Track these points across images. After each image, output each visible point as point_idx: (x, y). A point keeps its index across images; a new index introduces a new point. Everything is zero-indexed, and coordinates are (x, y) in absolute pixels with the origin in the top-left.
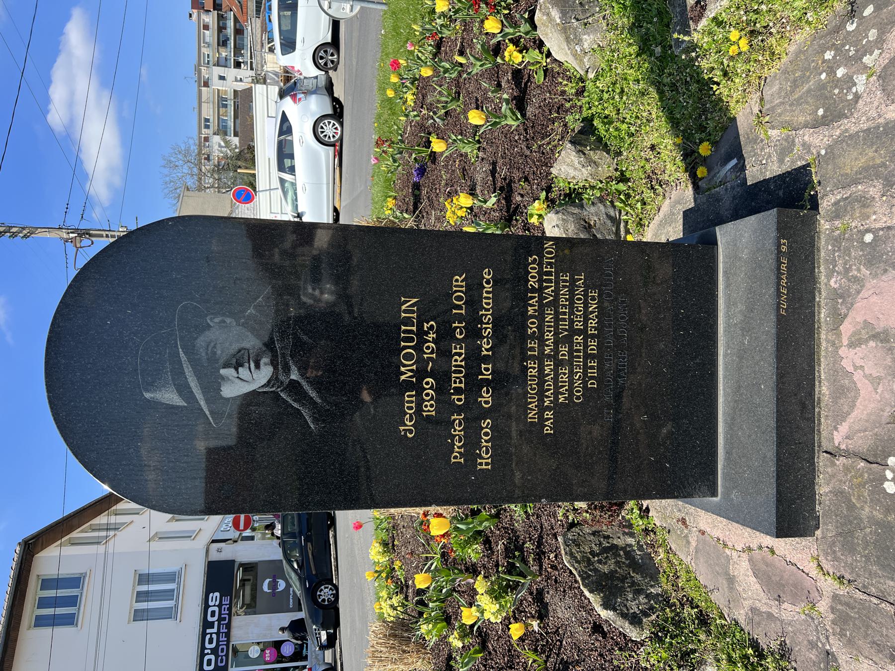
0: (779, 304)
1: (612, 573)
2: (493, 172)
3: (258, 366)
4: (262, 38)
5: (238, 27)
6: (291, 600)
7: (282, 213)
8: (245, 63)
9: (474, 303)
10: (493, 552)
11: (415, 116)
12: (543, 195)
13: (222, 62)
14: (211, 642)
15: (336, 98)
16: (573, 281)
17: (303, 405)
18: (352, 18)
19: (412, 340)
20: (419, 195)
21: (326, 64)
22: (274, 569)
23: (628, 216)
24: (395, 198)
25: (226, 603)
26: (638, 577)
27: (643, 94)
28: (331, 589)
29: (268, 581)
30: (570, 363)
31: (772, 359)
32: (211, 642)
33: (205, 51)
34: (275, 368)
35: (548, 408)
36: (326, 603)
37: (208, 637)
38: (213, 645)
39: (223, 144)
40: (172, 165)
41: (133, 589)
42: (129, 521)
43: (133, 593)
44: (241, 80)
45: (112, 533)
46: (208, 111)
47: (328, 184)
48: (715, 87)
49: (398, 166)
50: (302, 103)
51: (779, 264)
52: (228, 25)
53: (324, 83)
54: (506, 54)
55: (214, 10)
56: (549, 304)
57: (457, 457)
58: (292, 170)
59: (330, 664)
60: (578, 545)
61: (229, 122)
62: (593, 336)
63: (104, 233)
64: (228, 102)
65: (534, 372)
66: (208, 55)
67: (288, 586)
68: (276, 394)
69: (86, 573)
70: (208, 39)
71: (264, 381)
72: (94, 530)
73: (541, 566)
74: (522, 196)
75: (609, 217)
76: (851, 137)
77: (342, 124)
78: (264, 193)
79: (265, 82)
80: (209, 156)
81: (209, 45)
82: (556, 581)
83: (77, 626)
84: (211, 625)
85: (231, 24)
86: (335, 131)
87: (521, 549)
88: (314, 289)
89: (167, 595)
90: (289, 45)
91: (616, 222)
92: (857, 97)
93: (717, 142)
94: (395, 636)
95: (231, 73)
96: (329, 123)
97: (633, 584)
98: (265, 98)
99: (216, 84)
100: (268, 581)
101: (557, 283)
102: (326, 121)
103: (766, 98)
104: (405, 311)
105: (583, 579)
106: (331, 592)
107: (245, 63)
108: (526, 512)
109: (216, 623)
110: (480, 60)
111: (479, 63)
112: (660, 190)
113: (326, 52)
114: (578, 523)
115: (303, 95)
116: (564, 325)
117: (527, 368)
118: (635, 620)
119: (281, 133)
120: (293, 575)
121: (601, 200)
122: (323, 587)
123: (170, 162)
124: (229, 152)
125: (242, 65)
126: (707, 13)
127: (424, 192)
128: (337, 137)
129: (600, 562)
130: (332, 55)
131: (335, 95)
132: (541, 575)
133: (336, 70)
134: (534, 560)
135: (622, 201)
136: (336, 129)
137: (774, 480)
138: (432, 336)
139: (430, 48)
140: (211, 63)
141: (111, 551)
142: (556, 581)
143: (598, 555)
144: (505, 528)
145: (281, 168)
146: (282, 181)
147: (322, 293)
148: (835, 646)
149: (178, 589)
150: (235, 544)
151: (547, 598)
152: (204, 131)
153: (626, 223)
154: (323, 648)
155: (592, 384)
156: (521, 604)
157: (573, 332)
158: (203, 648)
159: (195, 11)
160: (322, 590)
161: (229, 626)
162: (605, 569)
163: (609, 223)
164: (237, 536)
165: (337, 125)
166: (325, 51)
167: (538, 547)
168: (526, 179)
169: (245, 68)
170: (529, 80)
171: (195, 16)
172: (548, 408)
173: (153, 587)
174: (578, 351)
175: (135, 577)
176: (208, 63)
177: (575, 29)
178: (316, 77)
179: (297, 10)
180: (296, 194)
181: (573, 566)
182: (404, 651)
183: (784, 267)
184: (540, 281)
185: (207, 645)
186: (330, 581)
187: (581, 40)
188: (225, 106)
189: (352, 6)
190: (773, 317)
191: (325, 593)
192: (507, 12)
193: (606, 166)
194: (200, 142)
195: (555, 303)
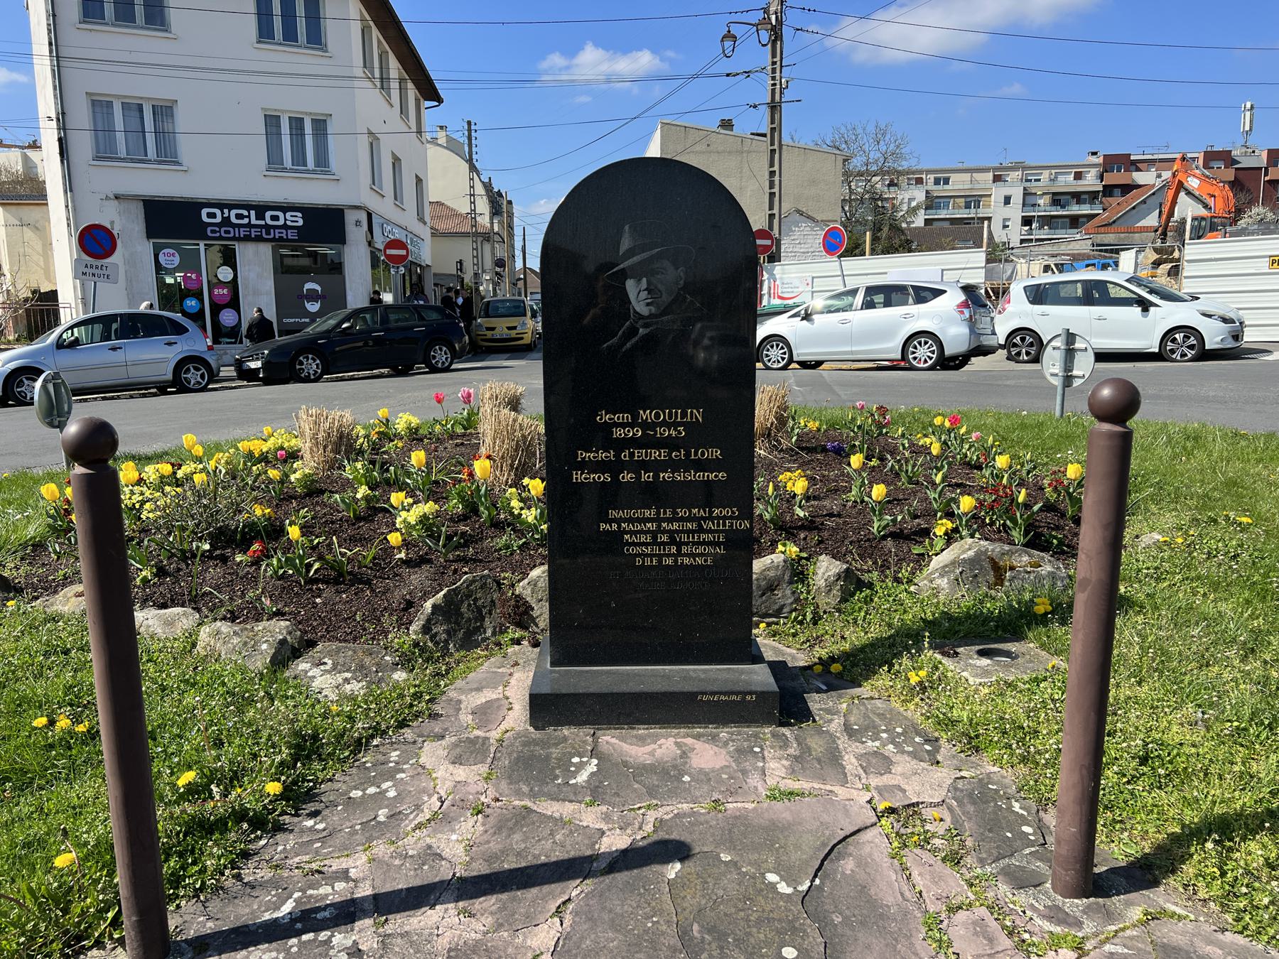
0: (706, 693)
1: (461, 615)
2: (831, 515)
3: (648, 304)
4: (1064, 255)
5: (1081, 220)
6: (293, 320)
7: (813, 292)
8: (1030, 232)
9: (700, 465)
10: (457, 522)
11: (903, 445)
12: (804, 555)
13: (1030, 200)
14: (239, 216)
15: (969, 360)
16: (718, 544)
17: (620, 338)
18: (1045, 378)
19: (670, 418)
20: (817, 453)
21: (1015, 345)
22: (333, 298)
23: (784, 625)
24: (819, 430)
25: (289, 234)
26: (460, 635)
27: (890, 626)
28: (316, 372)
29: (318, 288)
30: (655, 542)
31: (663, 690)
32: (239, 216)
33: (1045, 175)
34: (648, 317)
35: (619, 527)
36: (298, 367)
37: (245, 213)
38: (233, 220)
39: (914, 204)
40: (879, 136)
41: (306, 113)
42: (393, 101)
43: (302, 113)
44: (1005, 227)
45: (378, 84)
46: (959, 183)
47: (852, 353)
48: (886, 668)
49: (853, 431)
50: (957, 315)
51: (737, 693)
52: (1083, 206)
53: (985, 343)
54: (944, 521)
55: (1104, 186)
56: (700, 526)
57: (582, 455)
58: (869, 305)
59: (218, 375)
60: (481, 588)
61: (945, 212)
62: (676, 561)
63: (777, 59)
64: (973, 210)
65: (647, 514)
66: (1039, 180)
67: (313, 317)
68: (627, 317)
69: (326, 51)
70: (1061, 178)
71: (638, 309)
72: (380, 56)
73: (453, 561)
74: (805, 539)
75: (782, 607)
76: (834, 742)
77: (932, 368)
78: (839, 268)
79: (988, 261)
80: (896, 185)
81: (1053, 180)
82: (443, 573)
83: (259, 42)
84: (260, 216)
85: (1085, 210)
86: (923, 359)
87: (466, 545)
88: (711, 338)
89: (300, 158)
90: (1038, 295)
91: (777, 613)
92: (863, 743)
93: (842, 677)
94: (341, 437)
95: (1015, 213)
96: (933, 352)
97: (455, 631)
98: (963, 266)
99: (998, 192)
100: (318, 288)
101: (716, 531)
102: (935, 348)
103: (873, 701)
104: (692, 412)
105: (454, 590)
106: (312, 372)
107: (1030, 232)
108: (500, 549)
109: (262, 223)
110: (939, 497)
111: (937, 496)
112: (805, 646)
113: (1031, 345)
114: (500, 588)
115: (968, 316)
116: (684, 538)
117: (650, 508)
118: (426, 629)
119: (917, 289)
120: (332, 322)
121: (797, 600)
122: (318, 361)
123: (884, 135)
124: (902, 213)
125: (1027, 228)
126: (946, 659)
127: (819, 456)
128: (914, 363)
129: (469, 605)
130: (1028, 353)
131: (973, 359)
132: (446, 561)
133: (1008, 359)
134: (458, 555)
135: (796, 618)
136: (926, 361)
137: (572, 691)
138: (674, 433)
139: (975, 458)
140: (1028, 184)
141: (357, 83)
142: (443, 573)
143: (475, 604)
144: (482, 532)
145: (871, 290)
146: (854, 292)
147: (706, 348)
148: (449, 740)
149: (308, 172)
150: (366, 244)
151: (425, 567)
152: (932, 177)
153: (777, 624)
154: (239, 364)
155: (639, 561)
156: (414, 546)
157: (679, 545)
158: (231, 206)
159: (1101, 160)
160: (314, 360)
161: (259, 239)
162: (464, 609)
163: (776, 607)
164: (376, 246)
165: (930, 362)
166: (1032, 343)
167: (471, 559)
168: (820, 542)
169: (1023, 233)
170: (917, 542)
171: (1094, 160)
172: (619, 527)
173: (309, 140)
174: (664, 550)
175: (322, 114)
176: (1027, 181)
177: (953, 571)
178: (994, 333)
179: (1085, 305)
180: (837, 311)
181: (464, 582)
182: (325, 447)
183: (734, 697)
184: (718, 518)
185: (234, 212)
186: (325, 372)
187: (943, 576)
188: (968, 206)
189: (1056, 375)
190: (695, 690)
191: (311, 365)
192: (987, 521)
193: (828, 601)
194: (913, 173)
195: (701, 530)
